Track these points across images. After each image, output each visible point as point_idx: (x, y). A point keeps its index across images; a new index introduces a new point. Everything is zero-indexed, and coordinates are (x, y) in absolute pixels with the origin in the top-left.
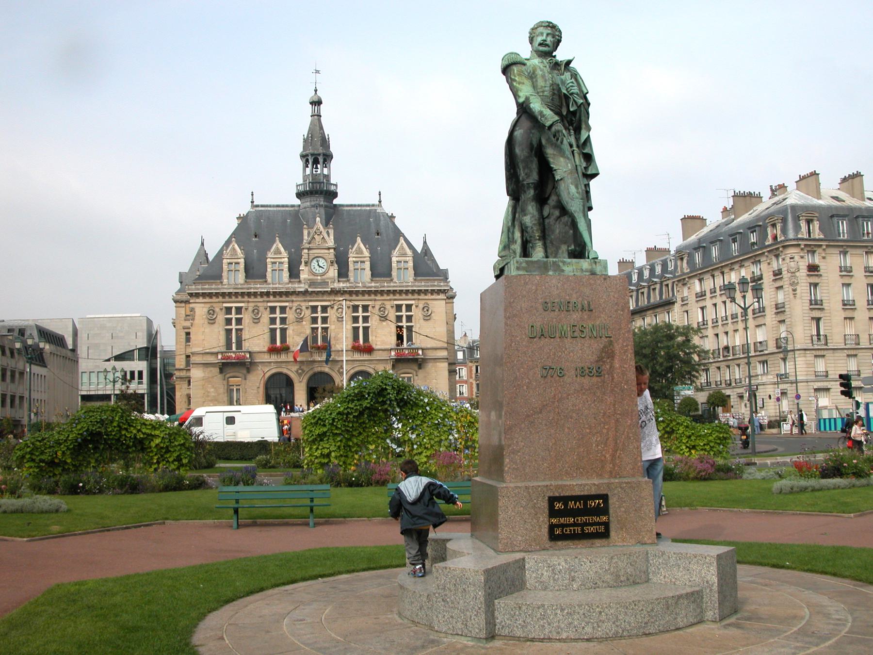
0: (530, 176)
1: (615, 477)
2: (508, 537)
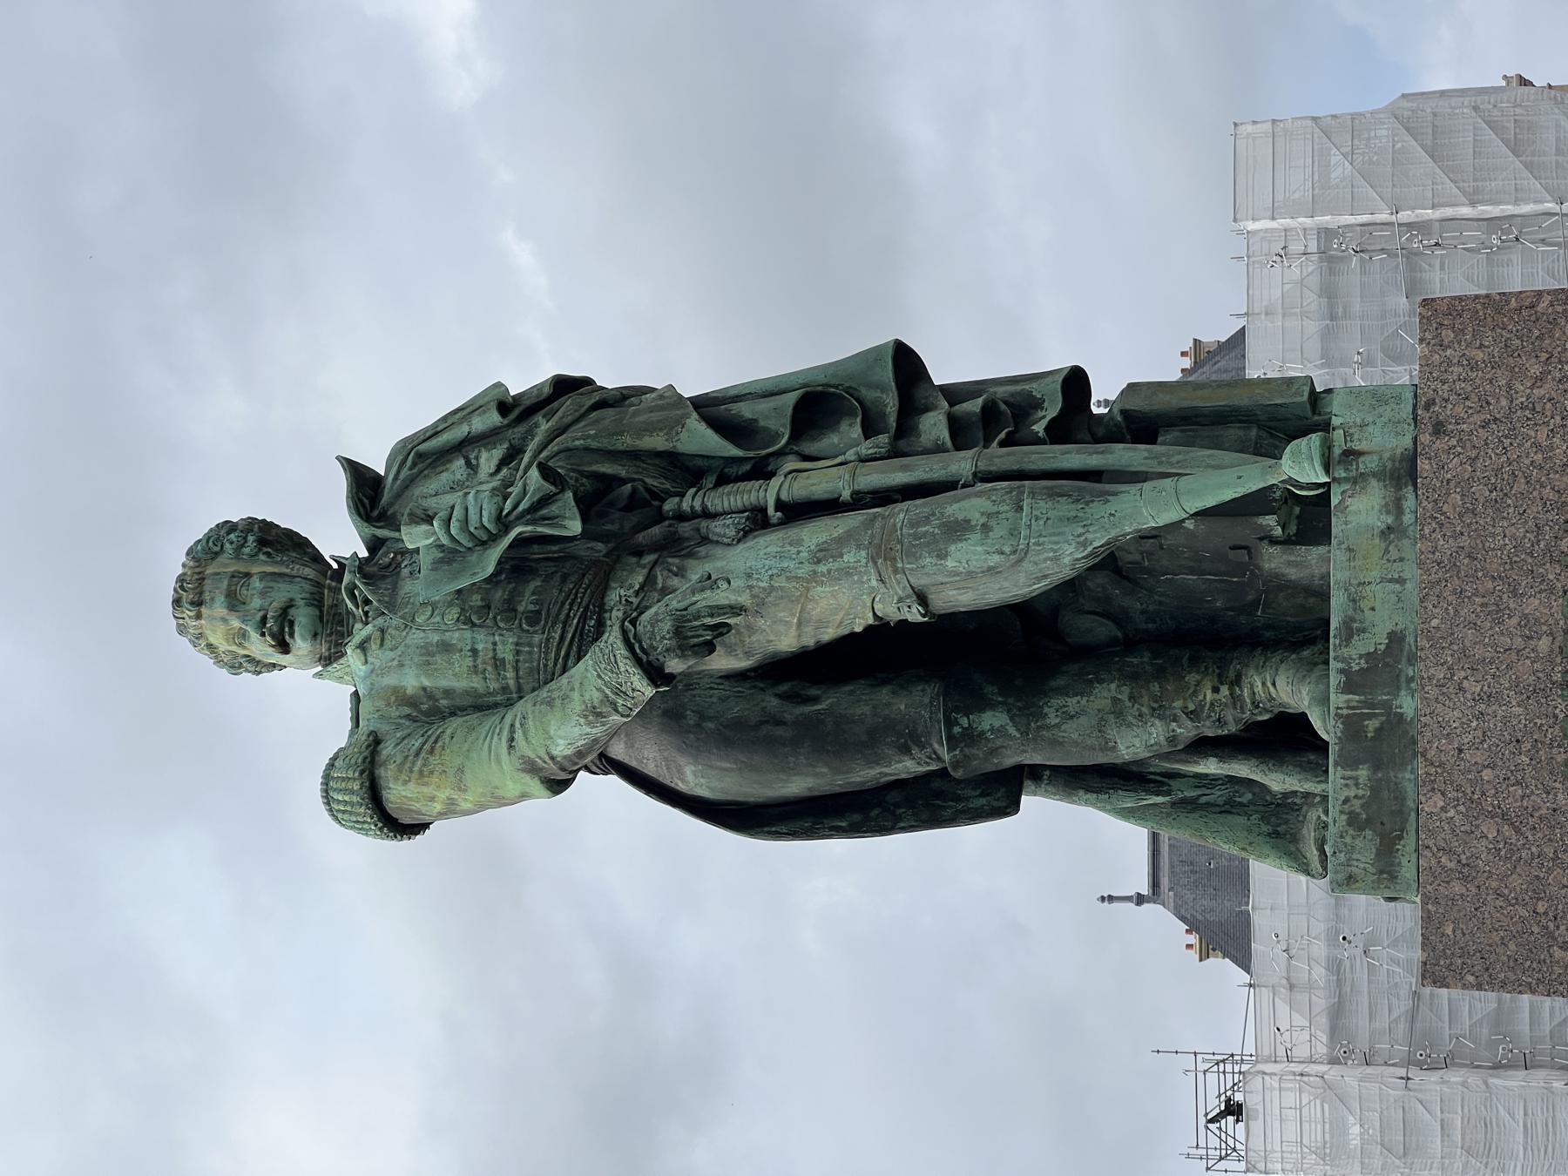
0: (914, 732)
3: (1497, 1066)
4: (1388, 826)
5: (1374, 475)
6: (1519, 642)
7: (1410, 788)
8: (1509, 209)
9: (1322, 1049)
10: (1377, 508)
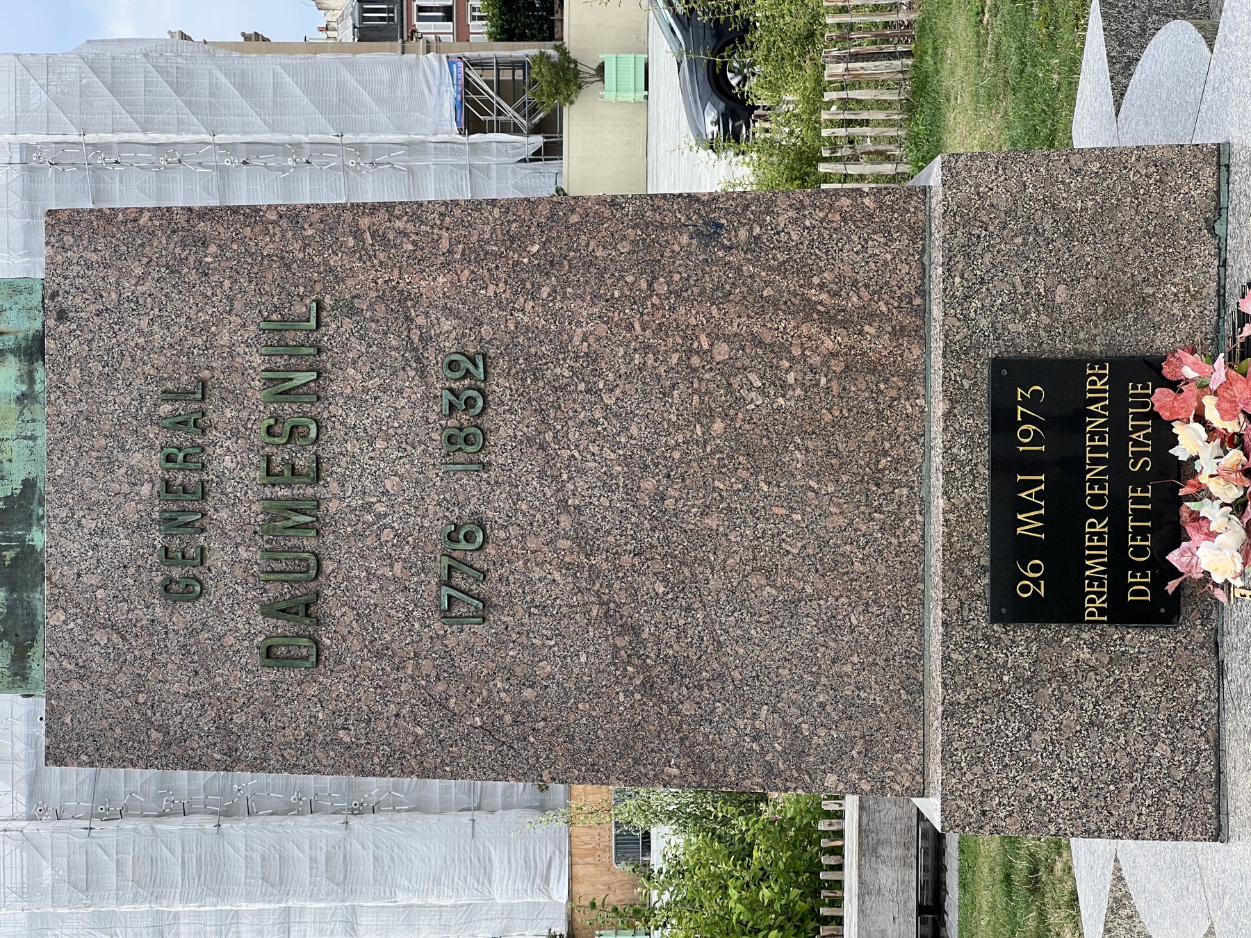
1: (922, 313)
2: (1157, 802)
3: (162, 815)
4: (22, 637)
5: (11, 351)
6: (126, 488)
7: (39, 605)
8: (173, 138)
9: (22, 809)
10: (13, 378)
